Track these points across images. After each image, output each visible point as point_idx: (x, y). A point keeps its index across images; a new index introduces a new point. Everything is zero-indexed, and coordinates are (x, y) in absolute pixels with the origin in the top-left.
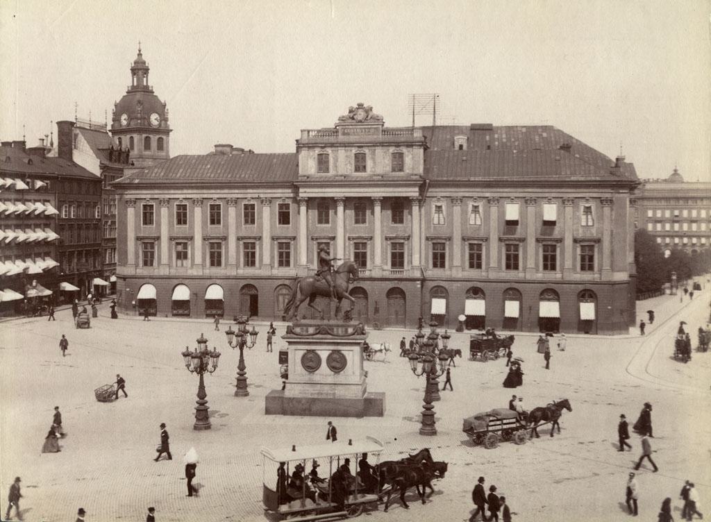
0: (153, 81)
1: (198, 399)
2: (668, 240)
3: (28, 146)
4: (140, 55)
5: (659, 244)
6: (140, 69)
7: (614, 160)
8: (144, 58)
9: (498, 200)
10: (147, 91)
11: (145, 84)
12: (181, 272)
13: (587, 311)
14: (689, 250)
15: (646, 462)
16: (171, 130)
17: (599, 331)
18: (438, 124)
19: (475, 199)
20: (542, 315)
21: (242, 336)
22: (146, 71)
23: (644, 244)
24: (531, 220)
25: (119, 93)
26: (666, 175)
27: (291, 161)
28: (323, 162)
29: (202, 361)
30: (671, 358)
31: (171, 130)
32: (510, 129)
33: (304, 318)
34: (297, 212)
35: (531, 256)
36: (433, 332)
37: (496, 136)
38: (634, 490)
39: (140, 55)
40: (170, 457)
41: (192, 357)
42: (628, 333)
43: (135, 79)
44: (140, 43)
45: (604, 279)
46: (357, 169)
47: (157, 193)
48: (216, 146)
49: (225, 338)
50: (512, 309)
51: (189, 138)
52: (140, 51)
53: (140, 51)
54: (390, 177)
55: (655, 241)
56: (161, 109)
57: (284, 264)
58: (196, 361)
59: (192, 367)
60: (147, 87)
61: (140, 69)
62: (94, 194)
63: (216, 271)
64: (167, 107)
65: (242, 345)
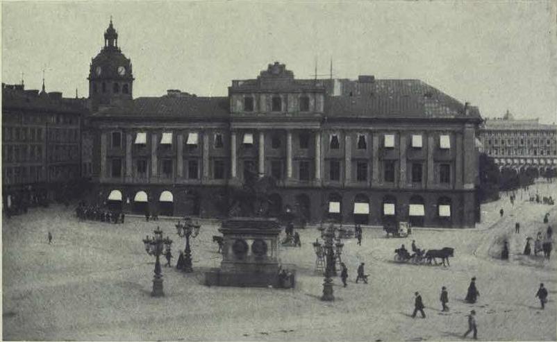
0: (121, 43)
1: (154, 274)
2: (516, 161)
3: (26, 88)
5: (496, 164)
6: (111, 34)
7: (464, 104)
9: (378, 131)
11: (115, 45)
12: (142, 181)
13: (445, 211)
14: (518, 170)
15: (419, 313)
17: (29, 210)
18: (318, 78)
19: (361, 131)
20: (355, 212)
21: (188, 229)
22: (116, 36)
23: (485, 162)
24: (403, 146)
25: (96, 52)
26: (501, 115)
28: (248, 104)
29: (157, 246)
32: (387, 82)
33: (235, 215)
35: (376, 170)
36: (331, 227)
37: (377, 86)
40: (475, 337)
41: (151, 244)
42: (474, 227)
43: (107, 41)
45: (457, 188)
46: (274, 109)
47: (122, 125)
48: (168, 91)
49: (176, 231)
50: (362, 208)
51: (147, 86)
55: (493, 161)
56: (127, 64)
58: (153, 246)
59: (150, 251)
61: (111, 34)
63: (116, 180)
65: (187, 235)
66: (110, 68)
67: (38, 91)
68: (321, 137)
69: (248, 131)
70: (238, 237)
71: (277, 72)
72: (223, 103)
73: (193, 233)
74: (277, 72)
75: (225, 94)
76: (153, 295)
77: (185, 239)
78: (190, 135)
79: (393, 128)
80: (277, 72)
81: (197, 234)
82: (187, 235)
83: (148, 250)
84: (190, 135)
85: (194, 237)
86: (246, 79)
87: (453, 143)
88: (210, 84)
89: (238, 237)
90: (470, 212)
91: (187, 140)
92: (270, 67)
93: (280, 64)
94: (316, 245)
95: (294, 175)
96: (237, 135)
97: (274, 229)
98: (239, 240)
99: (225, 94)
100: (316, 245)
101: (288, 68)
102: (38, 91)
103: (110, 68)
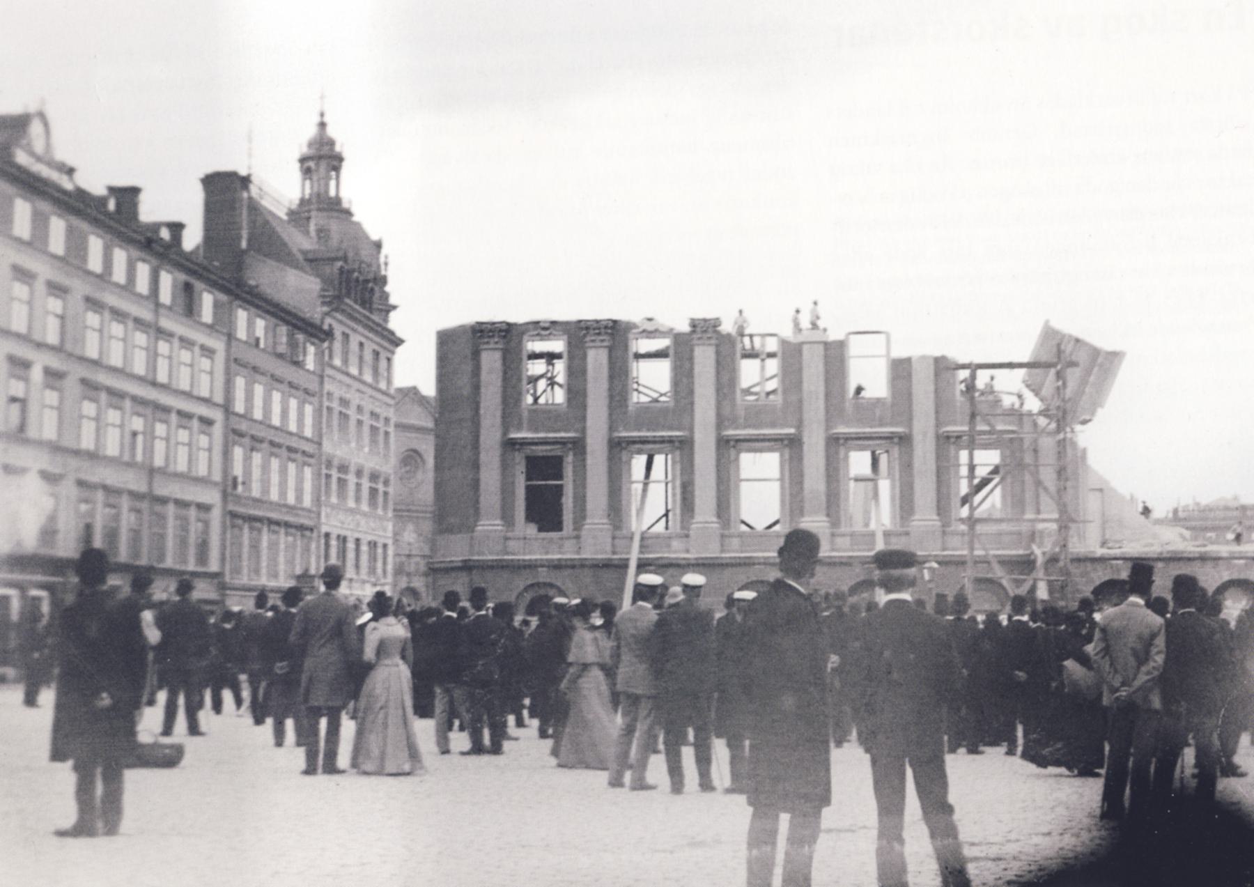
0: (352, 188)
4: (322, 125)
8: (331, 132)
10: (335, 208)
11: (332, 193)
16: (394, 307)
27: (102, 201)
30: (1047, 322)
31: (394, 307)
34: (871, 494)
38: (1090, 815)
39: (322, 125)
44: (322, 97)
52: (322, 115)
53: (322, 115)
54: (338, 218)
57: (320, 770)
60: (338, 200)
62: (142, 578)
64: (384, 251)
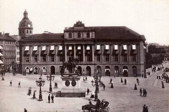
0: (29, 16)
1: (50, 86)
6: (25, 14)
28: (70, 36)
46: (78, 37)
61: (25, 14)
66: (24, 25)
67: (1, 33)
68: (94, 46)
69: (88, 45)
70: (67, 80)
71: (79, 24)
72: (62, 36)
73: (52, 79)
74: (79, 24)
75: (63, 32)
76: (39, 100)
77: (50, 81)
78: (26, 47)
79: (45, 44)
80: (79, 24)
81: (44, 85)
82: (50, 80)
83: (37, 85)
84: (26, 47)
85: (43, 86)
86: (70, 27)
87: (137, 47)
88: (58, 29)
89: (67, 80)
90: (143, 71)
91: (50, 49)
92: (77, 22)
93: (80, 21)
94: (92, 82)
95: (86, 60)
96: (67, 46)
97: (78, 77)
98: (67, 81)
99: (63, 32)
100: (92, 82)
101: (83, 23)
102: (1, 33)
103: (24, 25)
